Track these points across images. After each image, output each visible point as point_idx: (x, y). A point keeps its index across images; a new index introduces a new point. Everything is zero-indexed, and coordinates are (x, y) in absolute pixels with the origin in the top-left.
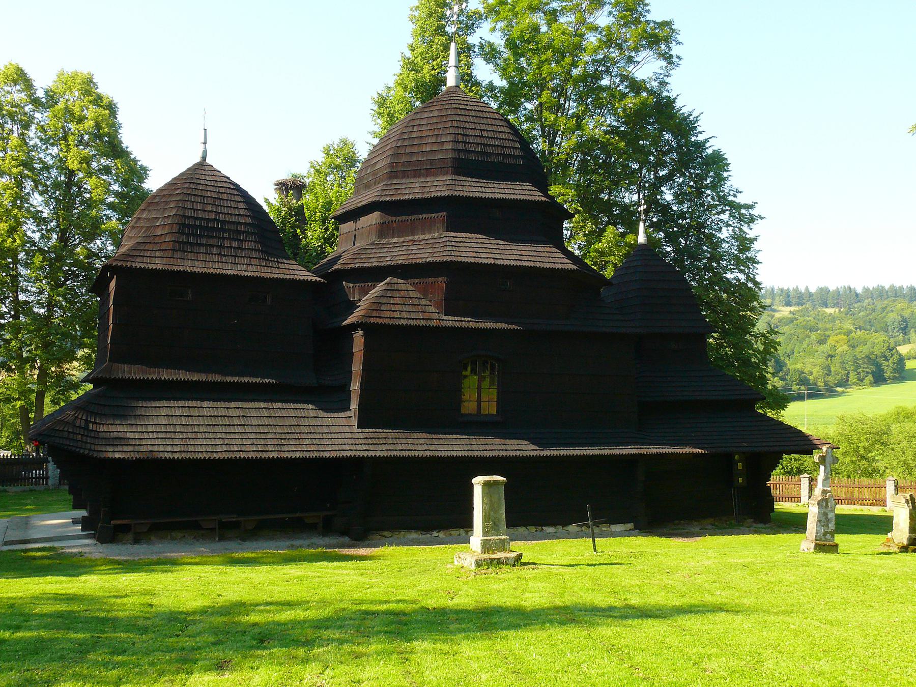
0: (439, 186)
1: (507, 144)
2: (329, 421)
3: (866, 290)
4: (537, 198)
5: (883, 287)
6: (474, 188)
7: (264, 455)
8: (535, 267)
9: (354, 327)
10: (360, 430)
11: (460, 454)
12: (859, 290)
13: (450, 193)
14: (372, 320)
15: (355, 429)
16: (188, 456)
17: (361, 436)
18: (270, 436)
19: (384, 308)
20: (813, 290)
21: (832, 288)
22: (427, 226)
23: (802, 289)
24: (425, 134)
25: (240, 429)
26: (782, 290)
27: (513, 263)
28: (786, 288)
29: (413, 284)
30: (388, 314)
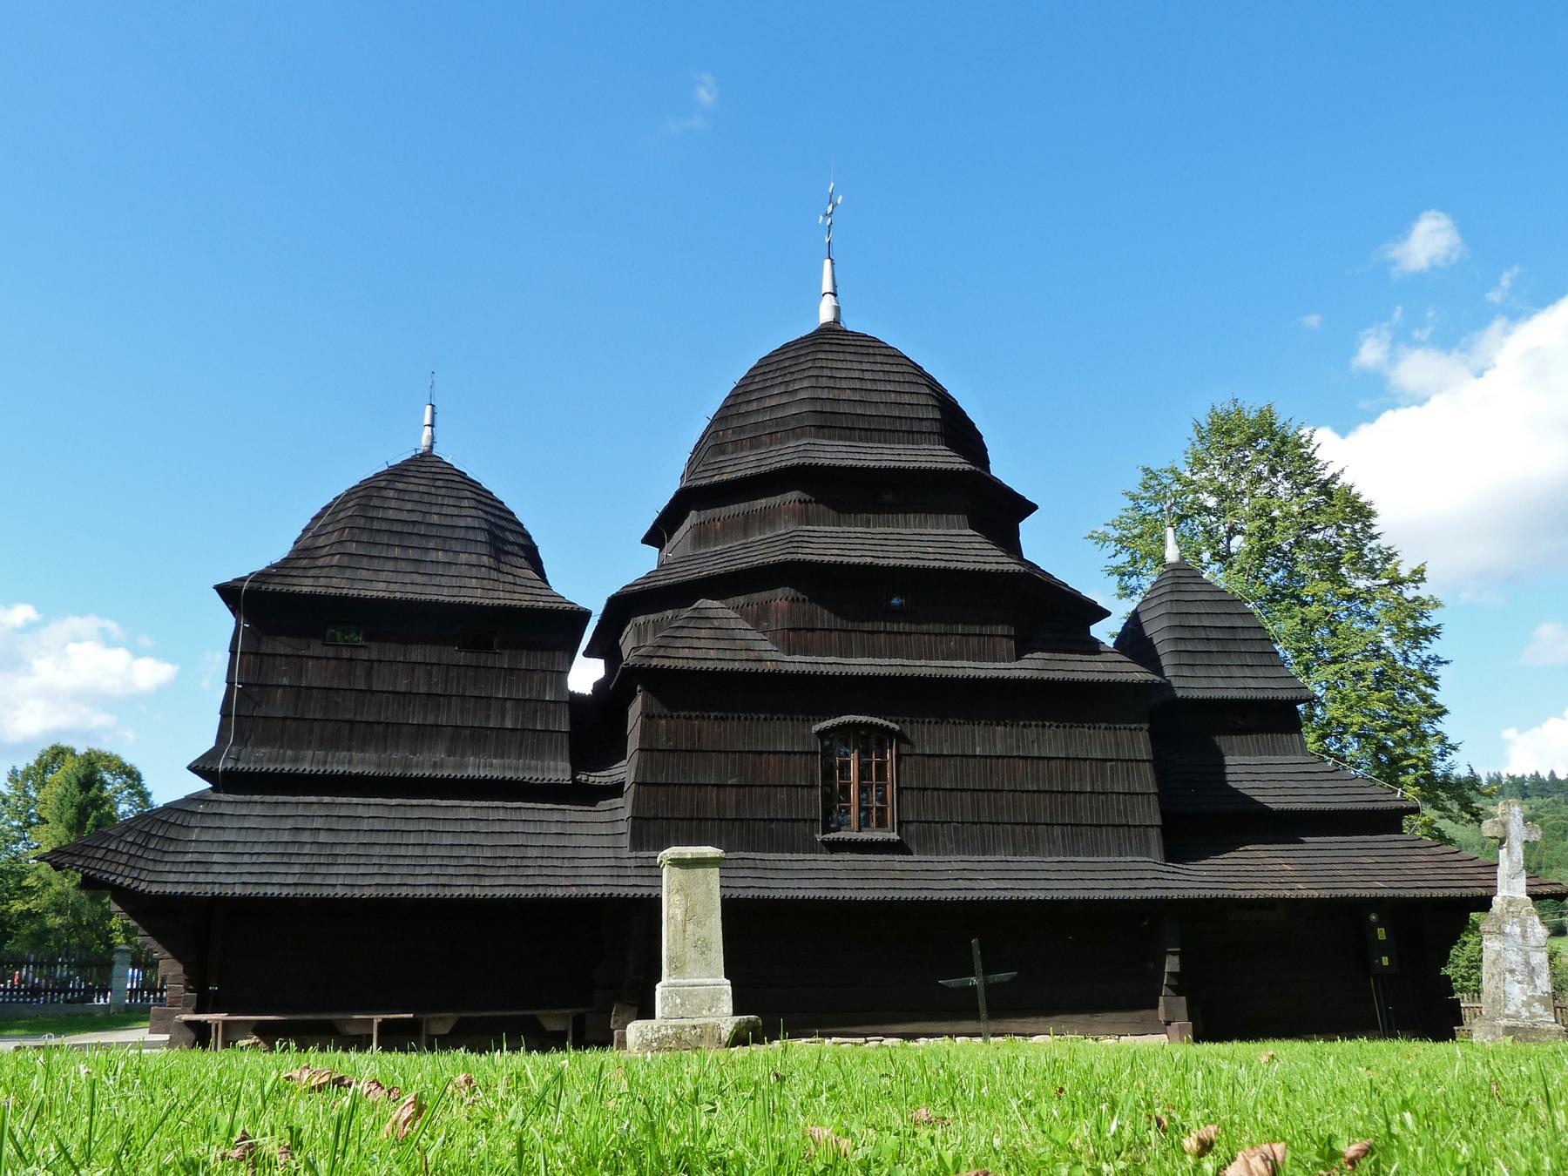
4: (956, 466)
7: (448, 892)
8: (946, 570)
10: (634, 854)
11: (810, 894)
13: (801, 461)
15: (626, 853)
16: (311, 891)
17: (633, 863)
18: (468, 861)
22: (767, 519)
23: (1545, 774)
25: (418, 851)
26: (1512, 778)
28: (1519, 775)
29: (736, 608)
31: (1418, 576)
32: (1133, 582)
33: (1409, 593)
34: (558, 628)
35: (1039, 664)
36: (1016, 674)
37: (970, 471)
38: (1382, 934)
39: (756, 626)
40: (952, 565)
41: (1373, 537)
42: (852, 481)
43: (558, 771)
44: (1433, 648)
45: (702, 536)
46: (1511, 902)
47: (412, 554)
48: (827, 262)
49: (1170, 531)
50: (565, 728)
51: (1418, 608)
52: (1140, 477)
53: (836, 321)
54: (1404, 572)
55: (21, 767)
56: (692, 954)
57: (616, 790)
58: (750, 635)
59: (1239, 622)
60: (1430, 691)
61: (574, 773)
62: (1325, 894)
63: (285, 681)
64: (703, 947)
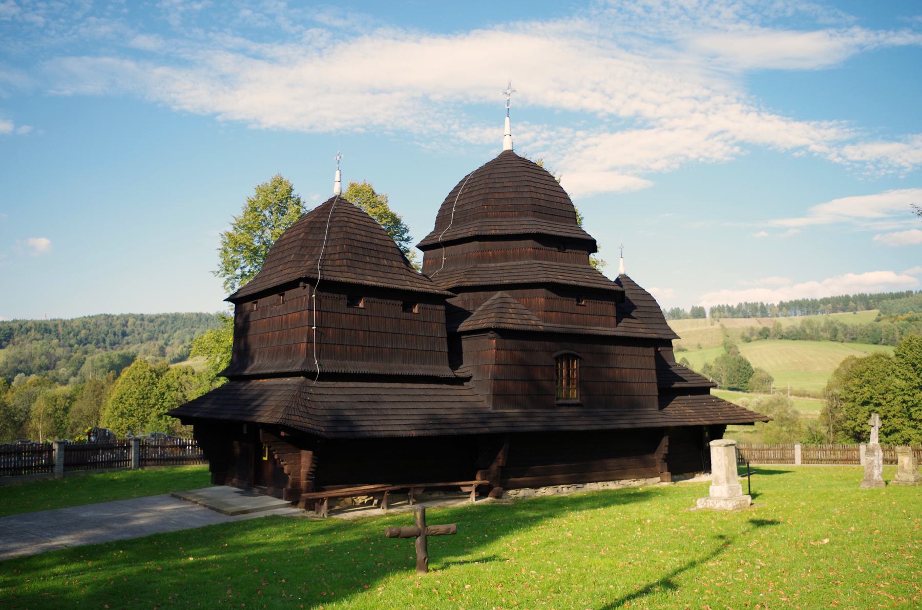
35: (623, 329)
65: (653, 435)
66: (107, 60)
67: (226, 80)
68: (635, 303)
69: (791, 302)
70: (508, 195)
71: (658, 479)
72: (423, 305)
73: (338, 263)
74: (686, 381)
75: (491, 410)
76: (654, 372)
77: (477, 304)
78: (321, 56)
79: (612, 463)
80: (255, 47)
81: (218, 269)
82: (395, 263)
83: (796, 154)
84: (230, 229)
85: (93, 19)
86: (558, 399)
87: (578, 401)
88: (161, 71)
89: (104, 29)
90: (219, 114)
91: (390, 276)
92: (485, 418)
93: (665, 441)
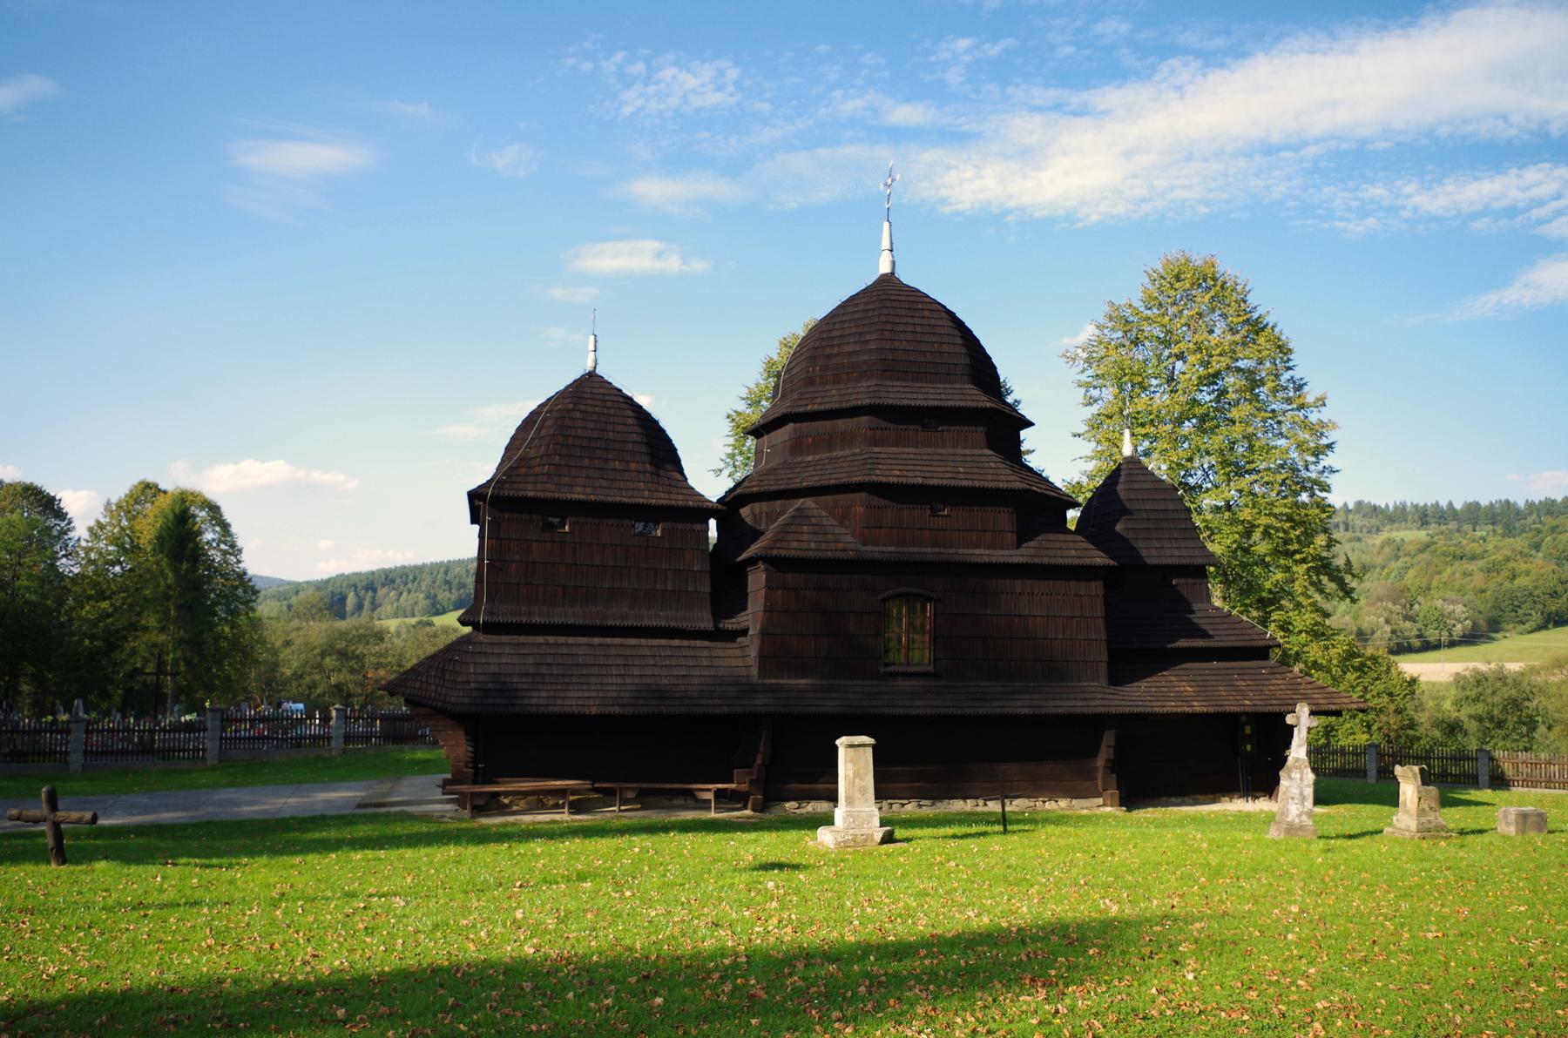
0: (861, 393)
1: (945, 339)
2: (720, 653)
3: (1530, 505)
4: (980, 405)
5: (1554, 501)
6: (900, 394)
9: (752, 561)
12: (1521, 504)
14: (775, 552)
19: (791, 537)
20: (1458, 506)
21: (1484, 502)
22: (847, 439)
23: (1444, 504)
24: (847, 332)
26: (1416, 507)
27: (945, 482)
30: (795, 544)
31: (1321, 402)
32: (1095, 393)
33: (1313, 417)
34: (699, 511)
35: (1032, 552)
36: (1016, 560)
37: (992, 409)
38: (1248, 730)
39: (841, 523)
40: (977, 484)
41: (1290, 368)
42: (895, 372)
43: (706, 623)
44: (1327, 460)
45: (797, 446)
46: (1297, 760)
47: (597, 463)
48: (886, 224)
49: (1127, 432)
50: (708, 589)
51: (1318, 430)
52: (1107, 309)
53: (893, 273)
54: (1310, 399)
55: (114, 500)
56: (857, 795)
57: (744, 632)
58: (837, 530)
59: (1171, 506)
60: (1324, 494)
61: (716, 622)
62: (1211, 710)
63: (517, 558)
64: (863, 791)
65: (1093, 725)
66: (851, 150)
67: (1028, 156)
68: (1128, 505)
69: (1530, 505)
70: (846, 349)
71: (1100, 801)
72: (669, 525)
73: (536, 470)
74: (1211, 637)
75: (755, 680)
76: (1101, 622)
77: (771, 518)
78: (1182, 98)
79: (1010, 768)
80: (1076, 99)
81: (722, 465)
82: (633, 466)
83: (1480, 224)
84: (741, 406)
85: (838, 93)
86: (887, 665)
87: (931, 669)
88: (930, 156)
89: (852, 105)
90: (1010, 211)
91: (621, 484)
92: (750, 689)
93: (1108, 739)
